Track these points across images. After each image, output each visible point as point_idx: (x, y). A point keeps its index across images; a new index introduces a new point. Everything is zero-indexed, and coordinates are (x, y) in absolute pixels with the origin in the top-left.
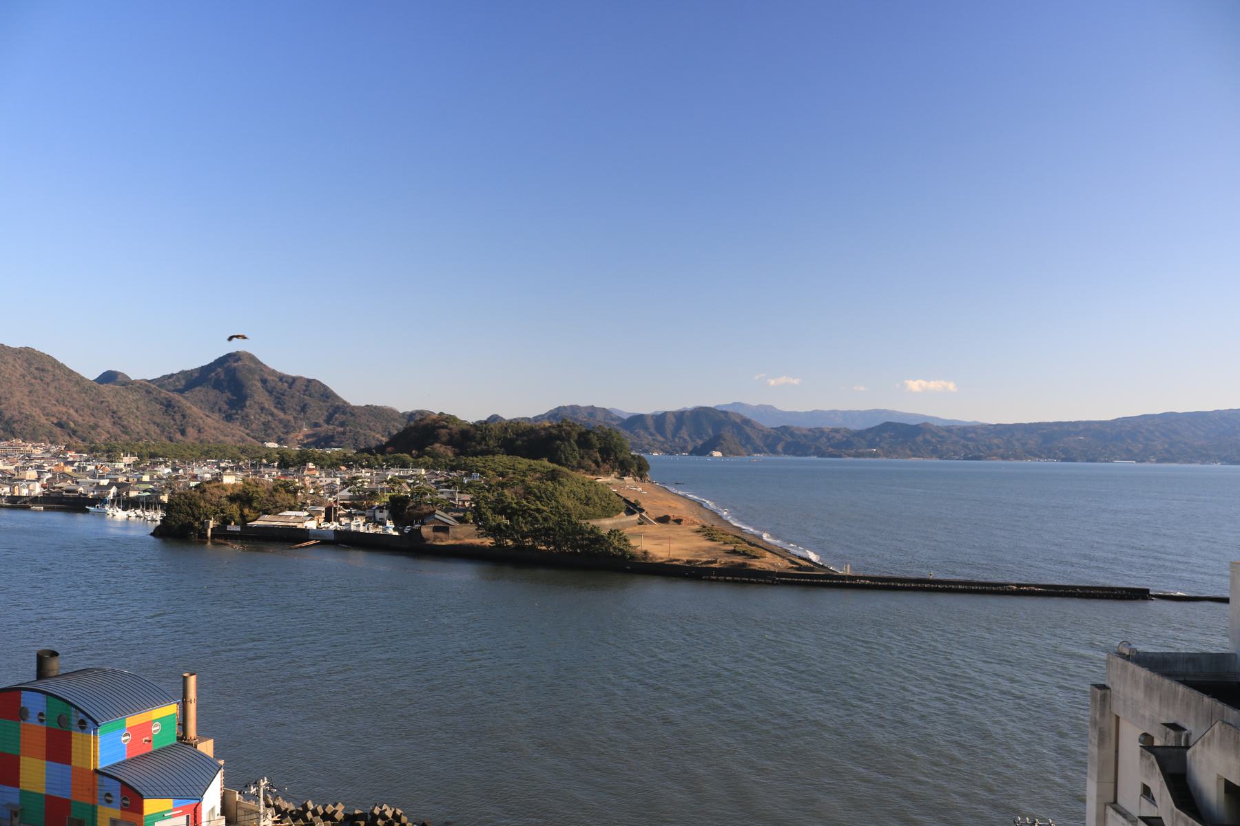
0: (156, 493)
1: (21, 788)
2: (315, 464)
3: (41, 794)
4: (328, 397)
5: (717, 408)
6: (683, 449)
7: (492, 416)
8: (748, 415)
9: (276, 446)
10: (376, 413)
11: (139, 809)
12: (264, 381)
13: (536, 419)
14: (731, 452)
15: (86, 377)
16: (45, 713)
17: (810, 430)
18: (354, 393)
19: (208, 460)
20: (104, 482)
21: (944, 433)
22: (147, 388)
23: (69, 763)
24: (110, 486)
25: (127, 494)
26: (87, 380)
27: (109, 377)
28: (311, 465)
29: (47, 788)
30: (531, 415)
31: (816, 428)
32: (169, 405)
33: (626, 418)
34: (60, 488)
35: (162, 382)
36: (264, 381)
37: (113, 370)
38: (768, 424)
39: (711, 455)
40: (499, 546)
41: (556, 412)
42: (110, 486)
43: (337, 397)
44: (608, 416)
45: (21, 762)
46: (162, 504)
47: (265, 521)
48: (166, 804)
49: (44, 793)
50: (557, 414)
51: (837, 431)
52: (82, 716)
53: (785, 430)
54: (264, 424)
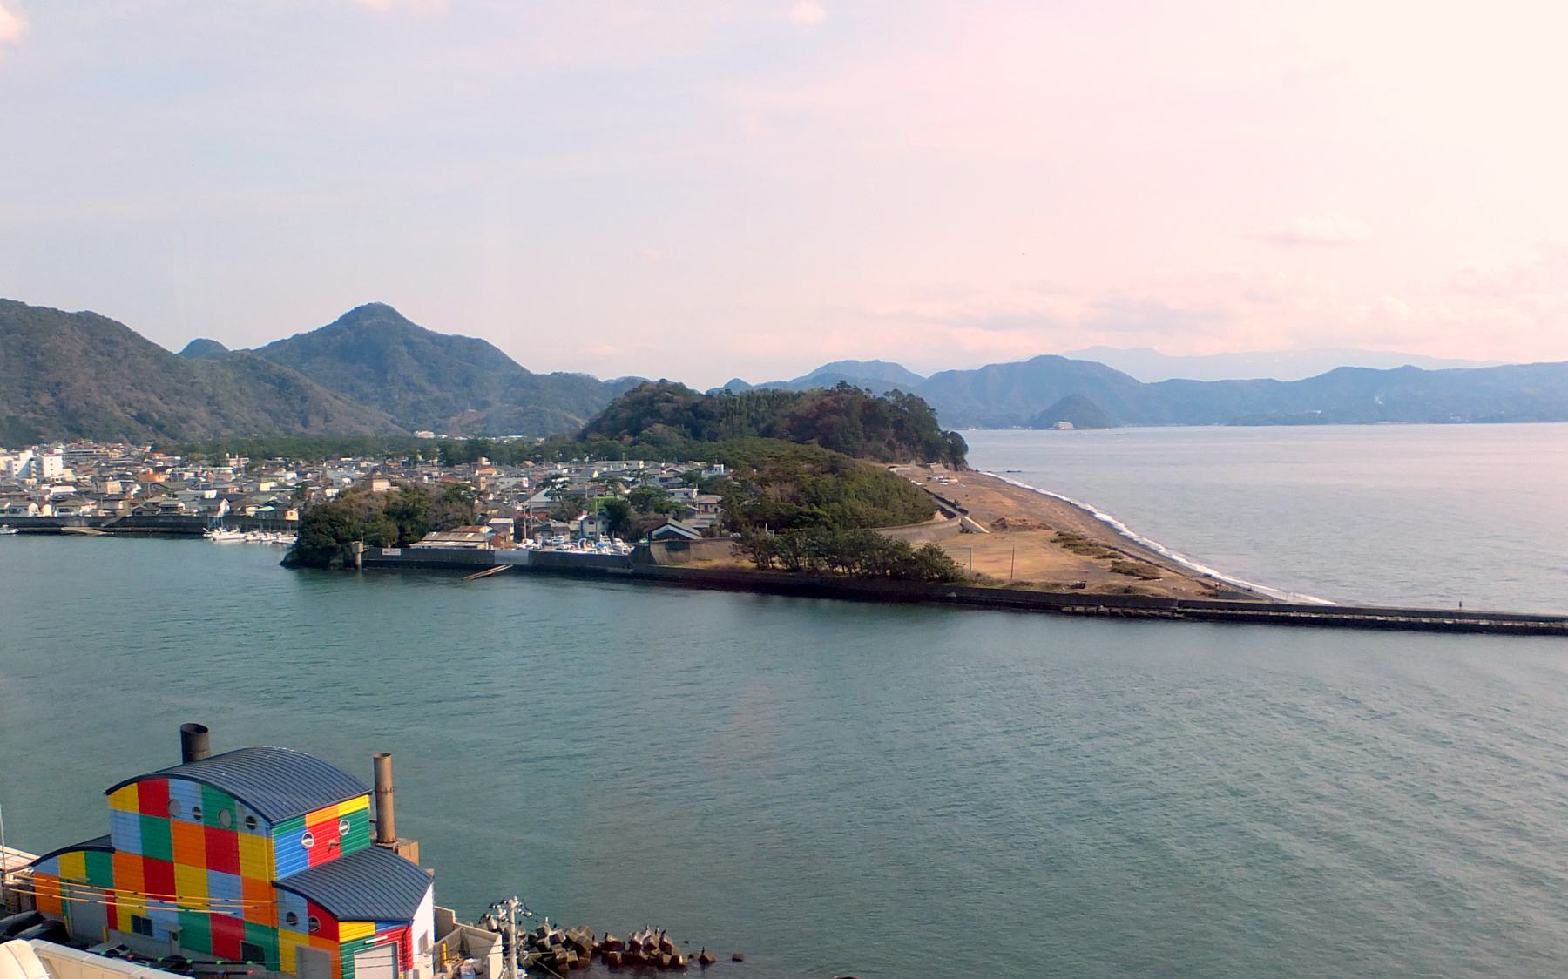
11: (334, 936)
13: (796, 382)
16: (201, 807)
20: (211, 494)
22: (249, 364)
25: (243, 510)
32: (283, 385)
33: (926, 375)
34: (154, 504)
35: (277, 349)
36: (410, 344)
42: (219, 498)
47: (435, 541)
52: (249, 812)
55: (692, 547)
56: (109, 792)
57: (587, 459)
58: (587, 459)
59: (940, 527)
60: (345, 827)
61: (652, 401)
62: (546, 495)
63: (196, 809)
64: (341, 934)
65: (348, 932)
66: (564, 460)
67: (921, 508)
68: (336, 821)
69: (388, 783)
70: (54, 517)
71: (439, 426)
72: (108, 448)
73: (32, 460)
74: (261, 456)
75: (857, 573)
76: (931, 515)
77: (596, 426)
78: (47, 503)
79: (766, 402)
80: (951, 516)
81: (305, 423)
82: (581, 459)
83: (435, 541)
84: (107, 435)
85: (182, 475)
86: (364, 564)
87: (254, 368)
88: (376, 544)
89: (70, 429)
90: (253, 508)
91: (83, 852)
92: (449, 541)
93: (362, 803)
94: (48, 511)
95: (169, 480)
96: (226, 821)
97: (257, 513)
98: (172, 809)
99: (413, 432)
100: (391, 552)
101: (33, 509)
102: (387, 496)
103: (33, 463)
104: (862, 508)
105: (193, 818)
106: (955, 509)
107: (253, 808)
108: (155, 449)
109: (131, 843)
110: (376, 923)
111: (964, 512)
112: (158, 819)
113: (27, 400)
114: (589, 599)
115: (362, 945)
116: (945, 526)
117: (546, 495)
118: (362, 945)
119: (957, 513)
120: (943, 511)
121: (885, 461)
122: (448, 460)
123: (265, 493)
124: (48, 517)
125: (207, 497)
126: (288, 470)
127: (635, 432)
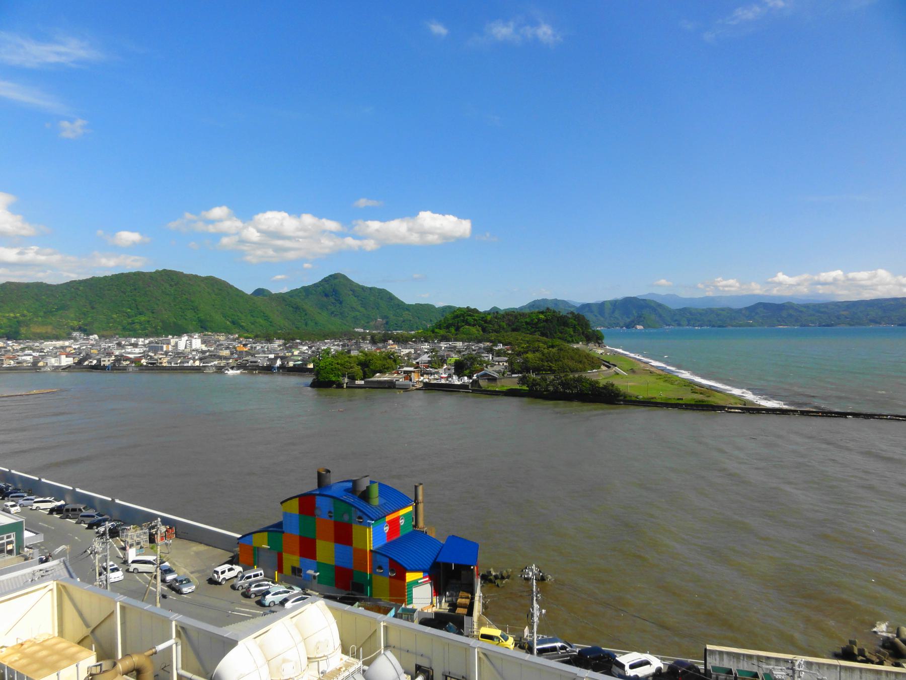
0: (305, 362)
1: (317, 561)
2: (393, 341)
3: (332, 566)
4: (392, 300)
5: (638, 297)
6: (617, 325)
7: (493, 308)
8: (659, 301)
9: (362, 330)
10: (426, 309)
11: (404, 578)
12: (353, 291)
13: (521, 308)
14: (649, 326)
15: (247, 293)
16: (333, 511)
17: (703, 310)
18: (409, 295)
19: (326, 341)
20: (272, 356)
21: (804, 309)
22: (281, 298)
23: (352, 545)
24: (276, 358)
25: (288, 363)
26: (247, 294)
27: (259, 292)
28: (391, 342)
29: (336, 561)
30: (517, 306)
31: (707, 309)
32: (297, 308)
33: (578, 306)
34: (246, 360)
35: (293, 293)
36: (353, 291)
37: (261, 288)
38: (673, 306)
39: (636, 328)
40: (564, 392)
41: (533, 304)
42: (276, 358)
43: (397, 299)
44: (567, 305)
45: (317, 544)
46: (310, 370)
47: (378, 377)
48: (419, 575)
49: (334, 564)
50: (534, 305)
51: (723, 310)
52: (359, 514)
53: (684, 310)
54: (354, 317)
55: (498, 381)
56: (282, 503)
57: (436, 341)
58: (436, 341)
59: (606, 372)
60: (402, 520)
61: (463, 315)
62: (429, 357)
63: (330, 512)
64: (407, 578)
65: (410, 577)
66: (426, 341)
67: (596, 363)
68: (398, 519)
69: (420, 498)
70: (200, 366)
71: (365, 326)
72: (218, 335)
73: (187, 340)
74: (289, 340)
75: (575, 393)
76: (599, 367)
77: (439, 326)
78: (197, 360)
79: (159, 331)
80: (609, 367)
81: (306, 324)
82: (434, 341)
83: (378, 377)
84: (217, 331)
85: (256, 347)
86: (347, 387)
87: (284, 300)
88: (353, 378)
89: (202, 327)
90: (292, 362)
91: (267, 533)
92: (386, 377)
93: (410, 509)
94: (197, 363)
95: (250, 349)
96: (346, 518)
97: (294, 365)
98: (317, 512)
99: (354, 328)
100: (358, 382)
101: (191, 363)
102: (357, 357)
103: (188, 342)
104: (571, 364)
105: (328, 517)
106: (610, 364)
107: (361, 511)
108: (240, 336)
109: (293, 531)
110: (423, 572)
111: (615, 366)
112: (310, 518)
113: (183, 314)
114: (447, 402)
115: (416, 583)
116: (608, 372)
117: (429, 357)
118: (416, 583)
119: (612, 366)
120: (604, 365)
121: (569, 342)
122: (374, 341)
123: (296, 356)
124: (197, 366)
125: (270, 357)
126: (304, 345)
127: (457, 329)
